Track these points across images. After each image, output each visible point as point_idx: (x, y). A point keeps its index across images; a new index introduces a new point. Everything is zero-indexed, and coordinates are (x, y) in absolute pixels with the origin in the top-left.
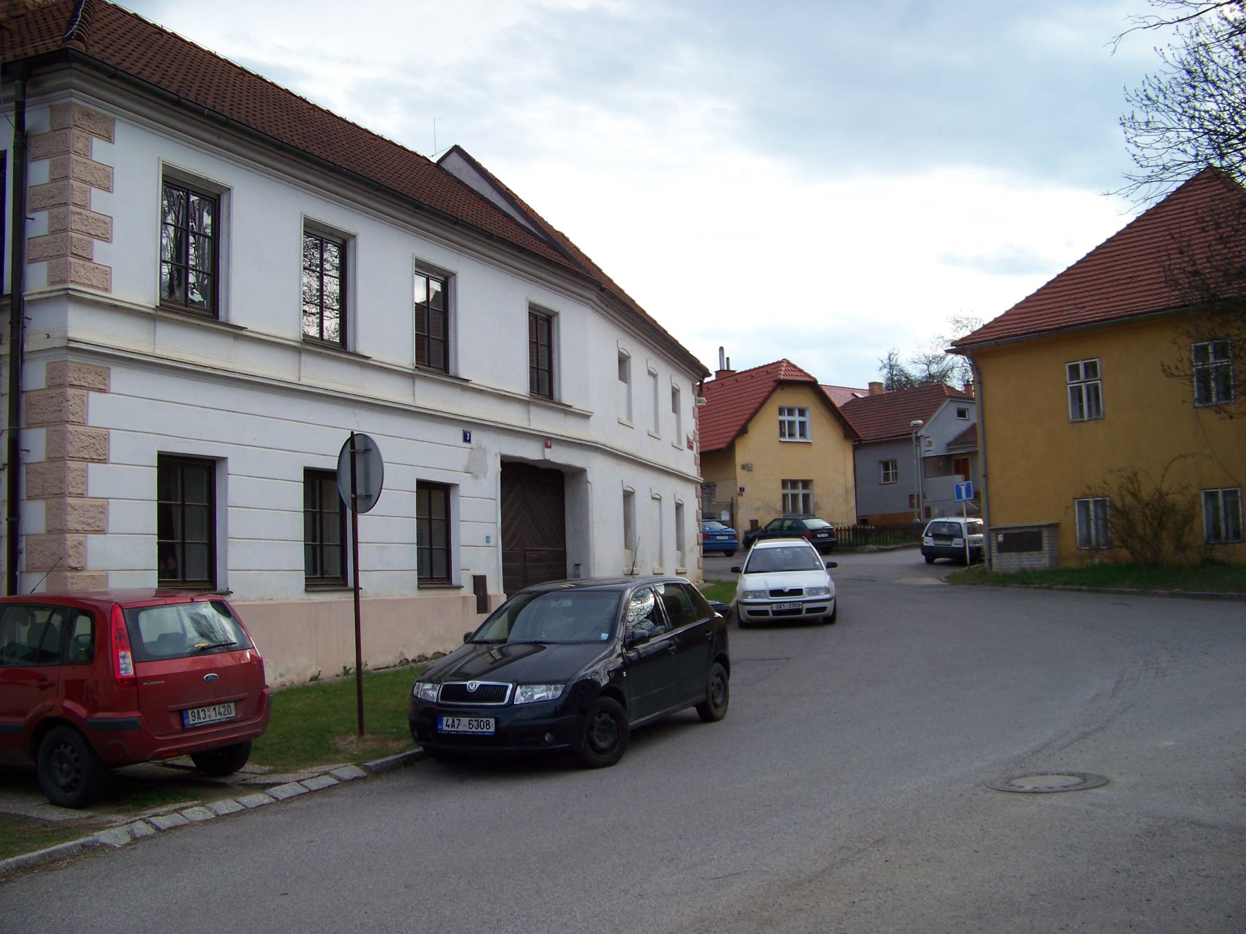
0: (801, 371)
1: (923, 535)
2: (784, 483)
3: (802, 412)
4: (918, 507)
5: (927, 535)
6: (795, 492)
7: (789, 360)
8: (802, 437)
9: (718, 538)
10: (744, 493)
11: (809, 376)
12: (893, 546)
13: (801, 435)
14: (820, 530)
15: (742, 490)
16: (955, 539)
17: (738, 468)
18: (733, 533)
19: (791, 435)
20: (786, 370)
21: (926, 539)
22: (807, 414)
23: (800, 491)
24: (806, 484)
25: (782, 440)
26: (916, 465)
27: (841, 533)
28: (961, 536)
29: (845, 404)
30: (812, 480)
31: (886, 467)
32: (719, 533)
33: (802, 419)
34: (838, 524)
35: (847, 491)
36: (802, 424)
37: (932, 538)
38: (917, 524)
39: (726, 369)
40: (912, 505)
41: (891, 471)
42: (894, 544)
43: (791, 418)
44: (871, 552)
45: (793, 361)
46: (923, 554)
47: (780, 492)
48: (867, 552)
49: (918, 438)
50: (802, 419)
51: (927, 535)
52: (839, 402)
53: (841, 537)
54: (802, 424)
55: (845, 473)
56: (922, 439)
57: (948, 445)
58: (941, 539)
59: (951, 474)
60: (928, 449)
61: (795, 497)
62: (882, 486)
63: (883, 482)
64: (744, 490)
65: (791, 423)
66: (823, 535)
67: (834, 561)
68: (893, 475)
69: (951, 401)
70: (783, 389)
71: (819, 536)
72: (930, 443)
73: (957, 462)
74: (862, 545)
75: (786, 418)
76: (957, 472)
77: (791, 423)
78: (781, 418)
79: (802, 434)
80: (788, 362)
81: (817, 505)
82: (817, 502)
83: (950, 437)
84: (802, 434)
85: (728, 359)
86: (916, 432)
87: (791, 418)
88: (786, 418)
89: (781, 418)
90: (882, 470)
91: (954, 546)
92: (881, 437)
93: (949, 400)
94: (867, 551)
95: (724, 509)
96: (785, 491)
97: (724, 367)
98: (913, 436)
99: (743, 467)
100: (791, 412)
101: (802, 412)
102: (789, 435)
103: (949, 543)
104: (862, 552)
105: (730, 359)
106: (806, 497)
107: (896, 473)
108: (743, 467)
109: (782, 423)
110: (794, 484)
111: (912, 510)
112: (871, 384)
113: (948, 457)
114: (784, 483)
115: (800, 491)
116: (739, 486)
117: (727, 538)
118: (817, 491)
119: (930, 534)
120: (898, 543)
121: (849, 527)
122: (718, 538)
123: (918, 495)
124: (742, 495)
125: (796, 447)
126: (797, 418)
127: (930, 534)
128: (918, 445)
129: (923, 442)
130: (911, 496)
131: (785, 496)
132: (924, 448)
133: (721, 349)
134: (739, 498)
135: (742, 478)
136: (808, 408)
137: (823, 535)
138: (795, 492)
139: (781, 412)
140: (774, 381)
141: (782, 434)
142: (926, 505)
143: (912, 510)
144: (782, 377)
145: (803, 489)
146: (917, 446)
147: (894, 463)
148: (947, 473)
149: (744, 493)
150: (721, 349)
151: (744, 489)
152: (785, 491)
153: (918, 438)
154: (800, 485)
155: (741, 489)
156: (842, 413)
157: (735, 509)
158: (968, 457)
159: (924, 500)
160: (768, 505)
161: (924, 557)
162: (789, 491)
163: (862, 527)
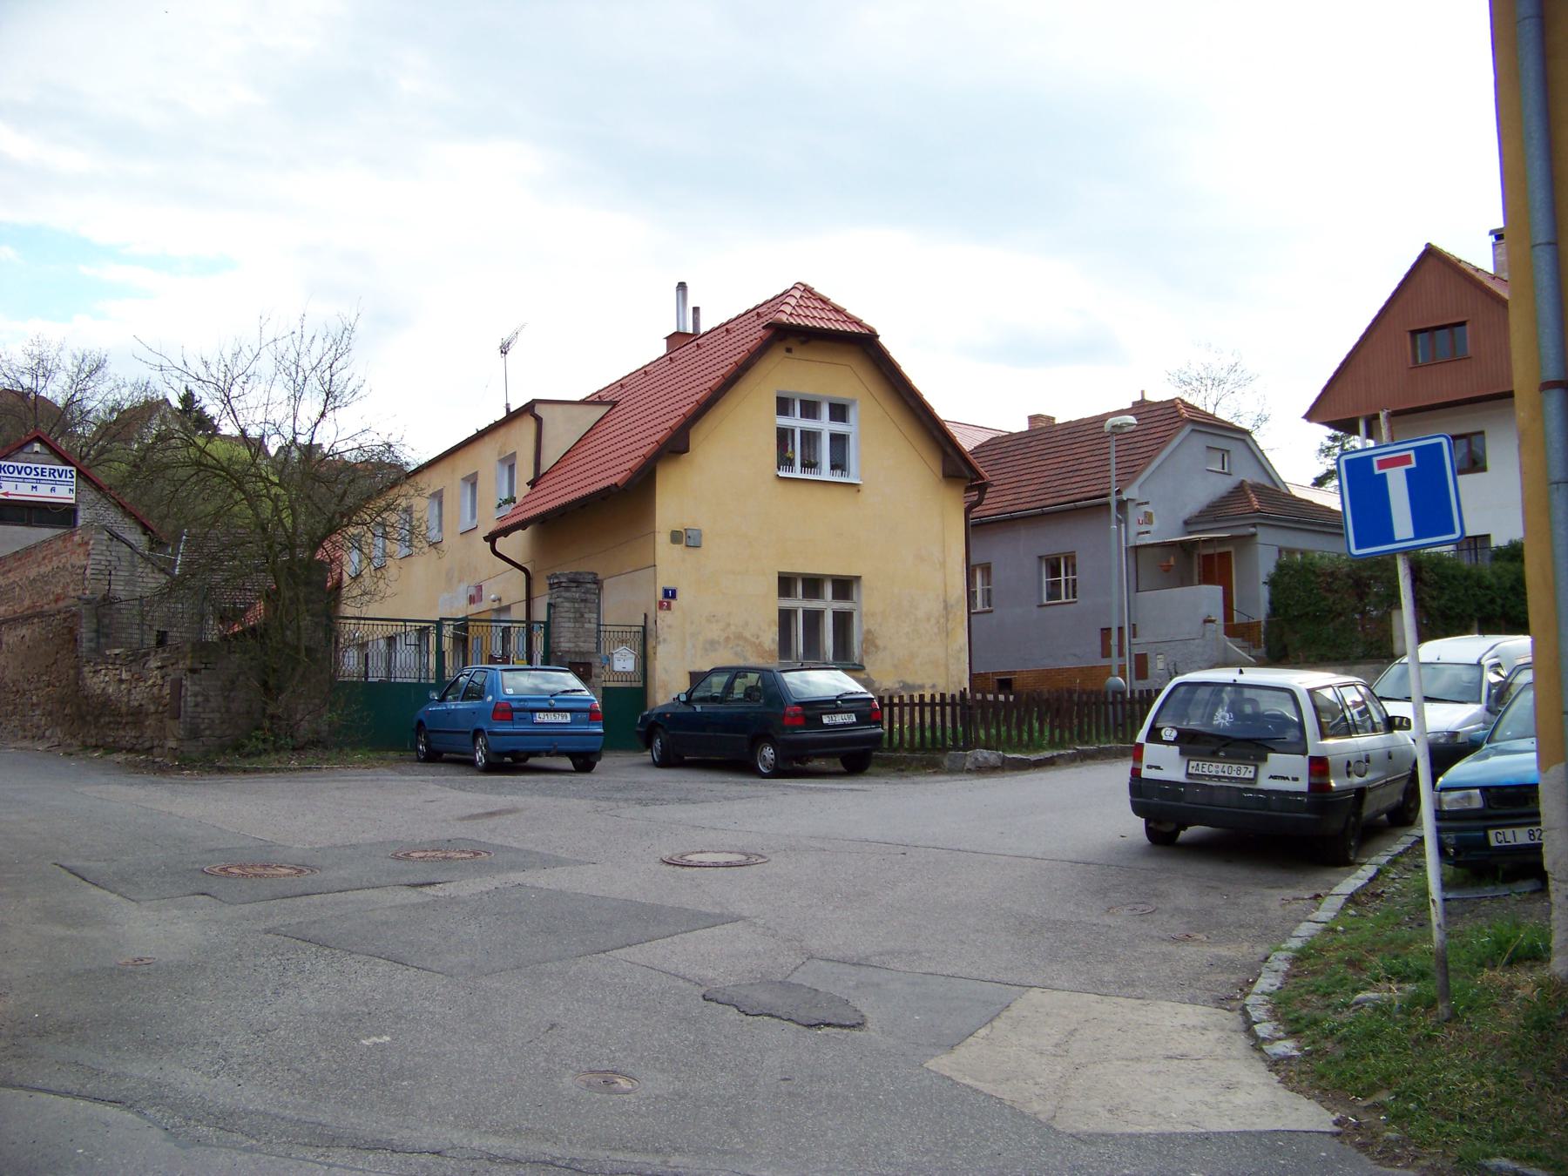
0: (838, 310)
1: (1141, 736)
2: (786, 584)
3: (839, 412)
4: (1121, 654)
5: (1154, 735)
6: (814, 604)
7: (811, 284)
8: (839, 472)
9: (541, 717)
10: (673, 603)
11: (858, 323)
12: (1047, 754)
13: (833, 467)
14: (833, 701)
15: (670, 594)
16: (1271, 756)
17: (662, 539)
18: (587, 706)
19: (810, 464)
20: (801, 297)
21: (1152, 752)
22: (852, 414)
23: (828, 604)
24: (844, 586)
25: (782, 474)
26: (1119, 565)
27: (1124, 709)
28: (1300, 747)
29: (975, 448)
30: (858, 578)
31: (1054, 570)
32: (545, 705)
33: (839, 427)
34: (922, 687)
35: (946, 608)
36: (839, 441)
37: (1176, 749)
38: (1115, 693)
39: (690, 330)
40: (1106, 653)
41: (1063, 578)
42: (1053, 744)
43: (809, 424)
44: (983, 770)
45: (820, 289)
46: (1138, 809)
47: (774, 603)
48: (969, 771)
49: (1122, 505)
50: (839, 427)
51: (1154, 735)
52: (967, 442)
53: (900, 726)
54: (839, 441)
55: (943, 564)
56: (1130, 506)
57: (1186, 523)
58: (1213, 756)
59: (1192, 584)
60: (1144, 528)
61: (813, 619)
62: (1044, 608)
63: (1045, 602)
64: (674, 596)
65: (810, 438)
66: (839, 719)
67: (1403, 606)
68: (1066, 584)
69: (1193, 430)
70: (789, 350)
71: (826, 720)
72: (1148, 518)
73: (1208, 559)
74: (955, 747)
75: (797, 422)
76: (1207, 579)
77: (810, 438)
78: (784, 421)
79: (839, 464)
80: (808, 290)
81: (870, 641)
82: (869, 632)
83: (1192, 507)
84: (839, 464)
85: (696, 310)
86: (1118, 492)
87: (809, 424)
88: (797, 422)
89: (784, 421)
90: (1044, 577)
91: (1264, 783)
92: (1043, 503)
93: (1188, 428)
94: (968, 765)
95: (623, 642)
96: (788, 603)
97: (685, 327)
98: (1113, 500)
99: (676, 537)
100: (810, 409)
101: (839, 412)
102: (803, 465)
103: (1247, 772)
104: (956, 770)
105: (702, 312)
106: (843, 622)
107: (1074, 580)
108: (676, 537)
109: (783, 435)
110: (813, 585)
111: (1105, 662)
112: (1032, 419)
113: (1185, 548)
114: (786, 584)
115: (828, 604)
116: (663, 582)
117: (568, 718)
118: (867, 607)
119: (1169, 734)
120: (1061, 744)
121: (953, 696)
122: (541, 717)
123: (1121, 629)
124: (669, 608)
125: (819, 492)
126: (825, 425)
127: (1169, 734)
128: (1123, 520)
129: (1134, 514)
130: (1106, 632)
131: (786, 617)
132: (1134, 528)
133: (682, 286)
134: (661, 614)
135: (670, 565)
136: (854, 401)
137: (839, 719)
138: (814, 604)
139: (783, 406)
140: (763, 328)
141: (784, 460)
142: (1136, 651)
143: (1105, 662)
144: (784, 318)
145: (834, 598)
146: (1119, 521)
147: (1070, 559)
148: (1184, 582)
149: (673, 603)
150: (682, 286)
151: (674, 592)
152: (788, 603)
153: (1122, 505)
154: (828, 590)
155: (666, 592)
156: (975, 462)
157: (651, 643)
158: (1231, 549)
159: (1134, 641)
160: (739, 637)
161: (1141, 822)
162: (799, 603)
163: (1002, 697)
